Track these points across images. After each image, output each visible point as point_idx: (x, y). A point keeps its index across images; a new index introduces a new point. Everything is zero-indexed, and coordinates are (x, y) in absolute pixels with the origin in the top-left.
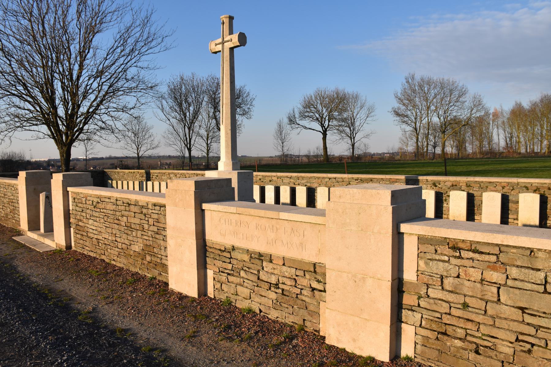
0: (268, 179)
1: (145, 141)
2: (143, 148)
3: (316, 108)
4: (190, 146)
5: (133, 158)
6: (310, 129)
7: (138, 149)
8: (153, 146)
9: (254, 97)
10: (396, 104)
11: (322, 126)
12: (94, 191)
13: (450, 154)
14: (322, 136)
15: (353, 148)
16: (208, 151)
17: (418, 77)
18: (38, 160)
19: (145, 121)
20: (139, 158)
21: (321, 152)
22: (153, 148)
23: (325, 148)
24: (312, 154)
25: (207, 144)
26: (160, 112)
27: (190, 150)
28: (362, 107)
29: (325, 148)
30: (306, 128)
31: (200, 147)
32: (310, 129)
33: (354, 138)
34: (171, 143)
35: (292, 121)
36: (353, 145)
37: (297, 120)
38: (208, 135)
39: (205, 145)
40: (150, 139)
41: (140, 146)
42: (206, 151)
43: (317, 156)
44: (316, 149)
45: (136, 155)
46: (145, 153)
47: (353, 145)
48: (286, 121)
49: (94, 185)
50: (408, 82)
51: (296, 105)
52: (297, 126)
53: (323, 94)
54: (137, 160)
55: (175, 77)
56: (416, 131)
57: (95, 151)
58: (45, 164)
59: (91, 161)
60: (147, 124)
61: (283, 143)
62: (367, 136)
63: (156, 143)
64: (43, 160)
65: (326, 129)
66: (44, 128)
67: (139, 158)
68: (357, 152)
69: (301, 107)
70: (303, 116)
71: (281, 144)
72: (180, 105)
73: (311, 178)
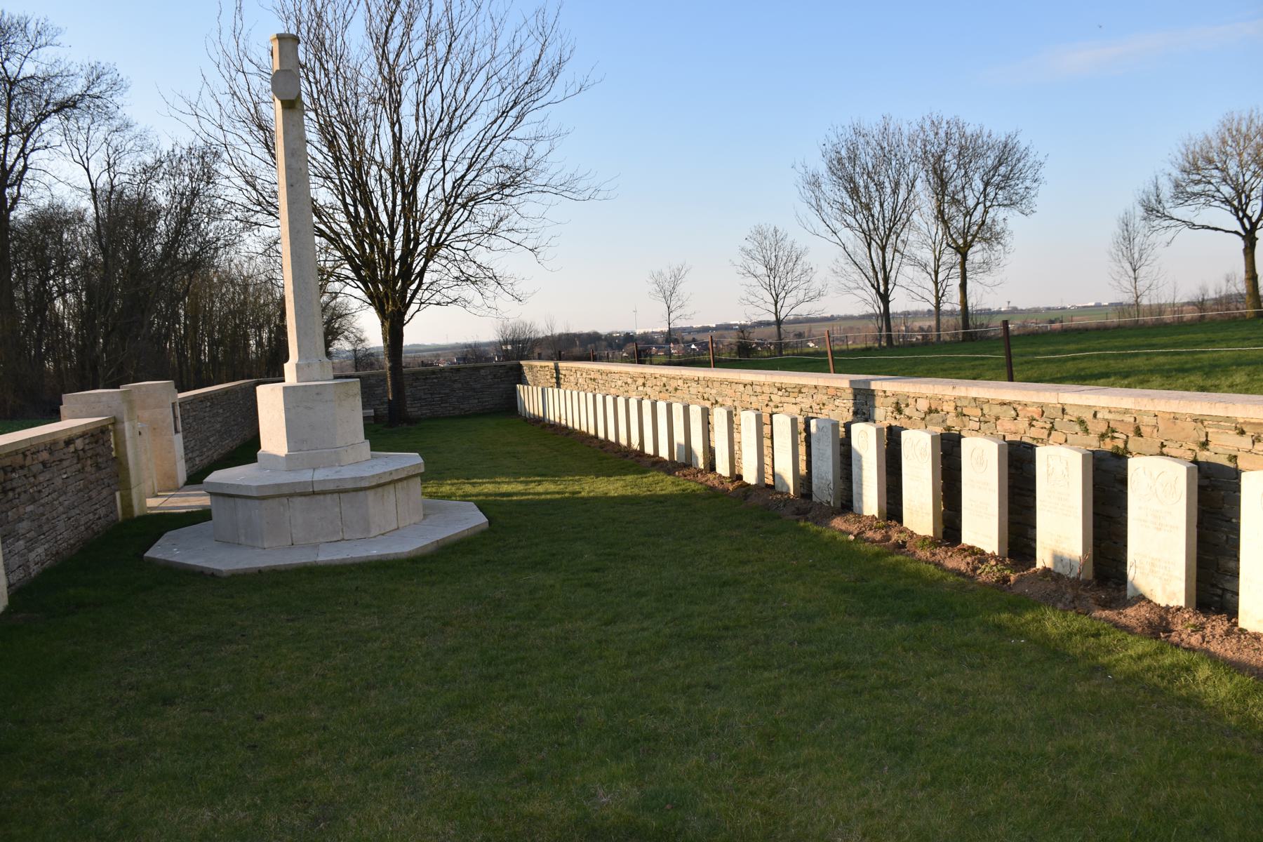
0: (674, 384)
2: (790, 300)
3: (1222, 171)
4: (886, 289)
5: (768, 324)
6: (1203, 227)
8: (811, 294)
9: (1040, 158)
11: (1239, 211)
12: (1041, 394)
13: (206, 245)
14: (1240, 244)
16: (938, 302)
20: (779, 322)
21: (1241, 287)
22: (811, 299)
23: (1252, 277)
24: (1212, 294)
25: (936, 283)
27: (885, 298)
29: (1252, 277)
30: (1193, 226)
32: (1203, 227)
34: (853, 285)
35: (1153, 210)
37: (1167, 205)
38: (937, 260)
39: (932, 286)
40: (804, 279)
41: (783, 294)
42: (933, 301)
43: (1225, 301)
44: (1224, 283)
45: (773, 318)
46: (793, 312)
48: (1140, 212)
51: (1160, 164)
52: (1166, 223)
53: (1244, 129)
54: (774, 328)
55: (840, 131)
57: (687, 310)
59: (757, 330)
60: (796, 245)
61: (1135, 270)
63: (817, 284)
65: (1254, 226)
67: (779, 322)
69: (1176, 173)
70: (1182, 194)
71: (1131, 273)
72: (854, 192)
73: (708, 382)
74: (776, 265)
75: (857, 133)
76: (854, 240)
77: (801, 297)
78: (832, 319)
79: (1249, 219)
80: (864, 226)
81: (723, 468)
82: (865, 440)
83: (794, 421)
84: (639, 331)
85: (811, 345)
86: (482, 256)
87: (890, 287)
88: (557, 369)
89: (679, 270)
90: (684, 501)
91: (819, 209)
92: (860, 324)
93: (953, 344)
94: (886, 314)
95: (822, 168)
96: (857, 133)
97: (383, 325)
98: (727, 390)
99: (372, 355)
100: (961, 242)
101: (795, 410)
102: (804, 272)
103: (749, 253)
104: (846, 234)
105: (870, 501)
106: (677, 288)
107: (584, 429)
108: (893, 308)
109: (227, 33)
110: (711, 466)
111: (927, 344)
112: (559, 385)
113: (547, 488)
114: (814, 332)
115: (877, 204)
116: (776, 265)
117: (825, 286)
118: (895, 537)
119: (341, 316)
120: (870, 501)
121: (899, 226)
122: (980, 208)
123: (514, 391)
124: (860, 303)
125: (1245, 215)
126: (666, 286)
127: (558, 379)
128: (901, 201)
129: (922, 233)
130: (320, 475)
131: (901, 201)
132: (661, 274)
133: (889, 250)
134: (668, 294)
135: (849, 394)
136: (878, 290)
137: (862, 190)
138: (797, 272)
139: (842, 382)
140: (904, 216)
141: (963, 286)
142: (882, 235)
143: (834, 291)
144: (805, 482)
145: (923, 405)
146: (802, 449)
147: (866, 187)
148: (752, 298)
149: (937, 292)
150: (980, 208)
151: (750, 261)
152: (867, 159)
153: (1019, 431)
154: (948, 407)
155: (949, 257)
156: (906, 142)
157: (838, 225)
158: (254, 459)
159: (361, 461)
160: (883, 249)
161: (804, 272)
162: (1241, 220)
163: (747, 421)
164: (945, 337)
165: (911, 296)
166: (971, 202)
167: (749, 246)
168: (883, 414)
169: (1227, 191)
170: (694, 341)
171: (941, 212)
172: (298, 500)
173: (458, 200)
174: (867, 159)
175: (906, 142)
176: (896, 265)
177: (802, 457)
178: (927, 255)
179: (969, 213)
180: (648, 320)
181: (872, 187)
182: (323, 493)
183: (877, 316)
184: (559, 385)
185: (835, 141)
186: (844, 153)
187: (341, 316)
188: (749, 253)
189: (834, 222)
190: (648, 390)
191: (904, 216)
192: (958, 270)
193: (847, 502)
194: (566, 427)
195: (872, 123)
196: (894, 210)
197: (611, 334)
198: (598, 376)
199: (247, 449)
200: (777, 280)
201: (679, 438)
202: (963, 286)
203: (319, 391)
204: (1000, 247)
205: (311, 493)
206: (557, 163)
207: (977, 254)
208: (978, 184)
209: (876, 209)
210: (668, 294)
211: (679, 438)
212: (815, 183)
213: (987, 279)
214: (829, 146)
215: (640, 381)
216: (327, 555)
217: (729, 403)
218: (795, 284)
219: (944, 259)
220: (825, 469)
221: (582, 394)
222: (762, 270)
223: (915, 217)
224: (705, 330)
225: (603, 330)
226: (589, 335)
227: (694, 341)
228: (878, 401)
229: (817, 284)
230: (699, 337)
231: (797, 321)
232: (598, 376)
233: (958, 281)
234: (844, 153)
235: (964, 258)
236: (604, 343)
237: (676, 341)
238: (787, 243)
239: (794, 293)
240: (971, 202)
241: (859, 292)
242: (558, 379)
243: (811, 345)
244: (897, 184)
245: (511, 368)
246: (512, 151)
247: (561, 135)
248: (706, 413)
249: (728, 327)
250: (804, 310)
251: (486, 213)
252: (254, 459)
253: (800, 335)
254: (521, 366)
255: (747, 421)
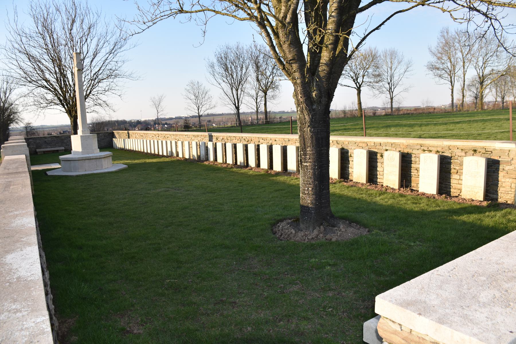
0: (167, 136)
1: (205, 102)
2: (204, 109)
4: (238, 105)
7: (198, 109)
8: (211, 106)
10: (433, 59)
11: (355, 80)
14: (356, 91)
15: (392, 102)
16: (257, 110)
17: (459, 29)
18: (148, 119)
19: (203, 86)
20: (200, 116)
21: (356, 107)
23: (360, 103)
24: (347, 109)
25: (257, 103)
26: (211, 78)
27: (238, 108)
28: (399, 63)
29: (360, 103)
31: (251, 105)
33: (392, 92)
36: (392, 99)
38: (257, 94)
39: (255, 104)
40: (209, 100)
41: (201, 106)
43: (351, 111)
47: (392, 99)
49: (488, 163)
50: (443, 36)
54: (198, 119)
55: (221, 47)
56: (452, 83)
58: (152, 123)
60: (206, 88)
62: (406, 90)
63: (213, 103)
64: (151, 119)
65: (360, 86)
66: (60, 107)
68: (395, 105)
72: (226, 69)
73: (176, 135)
74: (198, 95)
75: (228, 48)
76: (227, 88)
77: (208, 107)
78: (222, 114)
79: (359, 83)
80: (230, 82)
81: (180, 156)
82: (210, 145)
83: (197, 143)
84: (143, 119)
85: (214, 125)
86: (103, 97)
87: (240, 104)
88: (128, 133)
89: (162, 97)
90: (172, 162)
91: (214, 75)
92: (231, 116)
93: (263, 124)
94: (238, 114)
95: (215, 61)
96: (228, 48)
97: (71, 119)
98: (181, 137)
99: (34, 129)
100: (264, 88)
101: (197, 141)
102: (209, 98)
103: (188, 91)
104: (223, 85)
105: (212, 158)
106: (161, 104)
107: (139, 150)
108: (240, 111)
109: (12, 21)
110: (178, 155)
111: (252, 124)
112: (129, 138)
113: (137, 161)
114: (215, 120)
115: (235, 74)
116: (198, 95)
117: (217, 103)
118: (215, 163)
119: (14, 113)
120: (212, 158)
121: (243, 82)
122: (271, 77)
123: (112, 141)
124: (230, 109)
125: (357, 82)
126: (157, 103)
127: (129, 136)
128: (243, 73)
129: (250, 86)
130: (91, 155)
131: (243, 73)
132: (154, 98)
133: (239, 91)
134: (157, 105)
135: (208, 136)
136: (235, 105)
137: (230, 69)
138: (206, 98)
139: (206, 134)
140: (245, 78)
141: (265, 104)
142: (237, 85)
143: (220, 105)
144: (199, 157)
145: (221, 138)
146: (199, 150)
147: (231, 67)
148: (189, 108)
149: (257, 106)
150: (271, 77)
151: (189, 94)
152: (232, 56)
153: (235, 141)
154: (225, 138)
155: (261, 94)
156: (245, 52)
157: (221, 81)
158: (71, 153)
159: (97, 153)
160: (237, 90)
161: (209, 98)
162: (356, 84)
163: (186, 144)
164: (260, 122)
165: (248, 107)
166: (268, 74)
167: (188, 88)
168: (214, 140)
169: (352, 74)
170: (166, 124)
171: (257, 77)
172: (87, 161)
173: (96, 79)
174: (232, 56)
175: (245, 52)
176: (242, 96)
177: (199, 151)
178: (253, 93)
179: (267, 78)
180: (150, 116)
181: (233, 67)
182: (92, 159)
183: (234, 114)
184: (129, 138)
185: (220, 51)
186: (223, 55)
187: (14, 113)
188: (188, 91)
189: (220, 80)
190: (160, 138)
191: (245, 78)
192: (263, 98)
193: (207, 159)
194: (133, 150)
195: (233, 44)
196: (241, 76)
197: (131, 121)
198: (143, 135)
199: (69, 150)
200: (199, 101)
201: (169, 149)
202: (265, 104)
203: (89, 136)
204: (277, 91)
205: (90, 159)
206: (125, 69)
207: (270, 93)
208: (270, 68)
209: (235, 76)
210: (157, 105)
211: (169, 149)
212: (212, 66)
213: (274, 102)
214: (217, 53)
215: (157, 136)
216: (95, 172)
217: (182, 140)
218: (205, 102)
219: (259, 94)
220: (203, 152)
221: (139, 140)
222: (193, 97)
223: (249, 78)
224: (171, 119)
225: (128, 119)
226: (121, 121)
227: (166, 124)
228: (214, 137)
229: (213, 103)
230: (168, 122)
231: (208, 115)
232: (143, 135)
233: (264, 102)
234: (223, 55)
235: (266, 94)
236: (128, 125)
237: (159, 124)
238: (202, 87)
239: (205, 106)
240: (268, 74)
241: (228, 106)
242: (129, 136)
243: (214, 125)
244: (242, 67)
245: (110, 133)
246: (112, 66)
247: (128, 59)
248: (176, 143)
249: (180, 118)
250: (210, 112)
251: (103, 85)
252: (71, 153)
253: (209, 121)
254: (113, 133)
255: (186, 144)
